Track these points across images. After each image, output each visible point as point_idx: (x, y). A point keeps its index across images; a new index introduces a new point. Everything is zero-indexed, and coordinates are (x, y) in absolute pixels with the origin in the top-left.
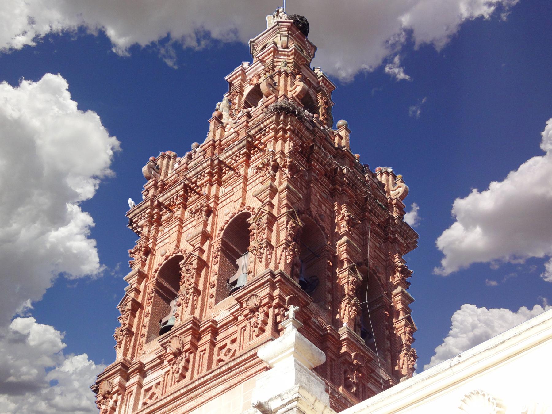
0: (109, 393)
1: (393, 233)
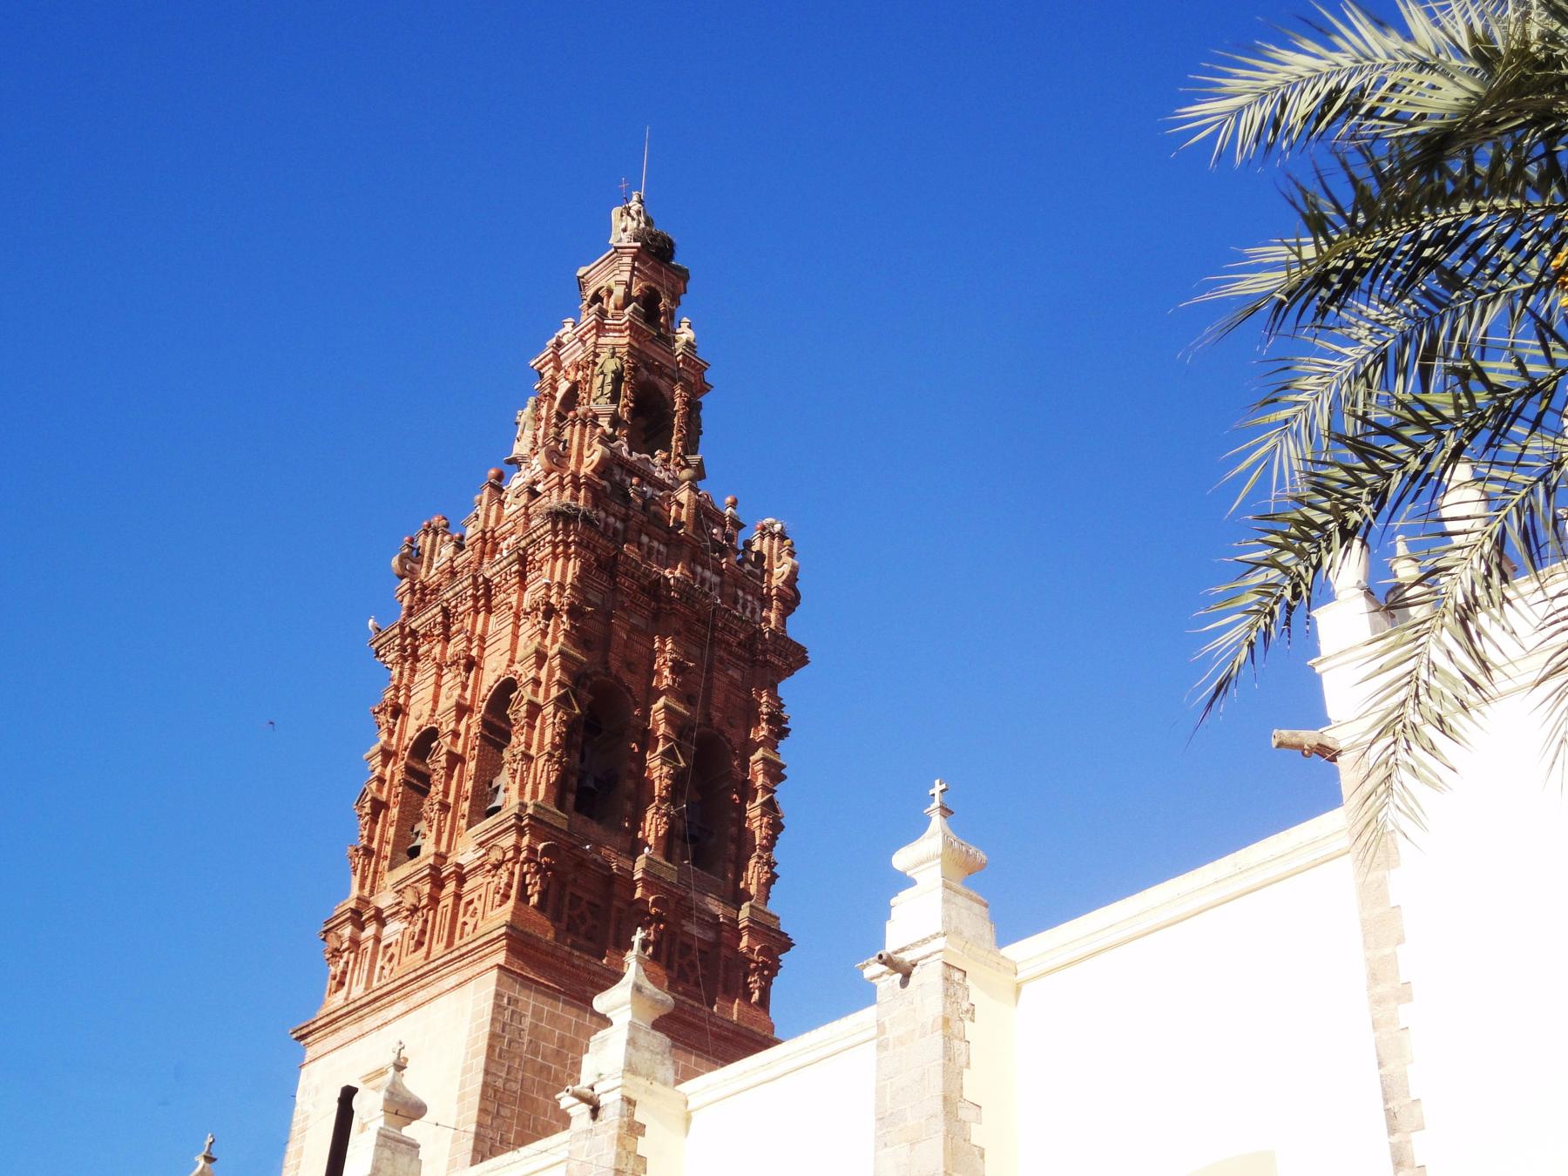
0: (337, 950)
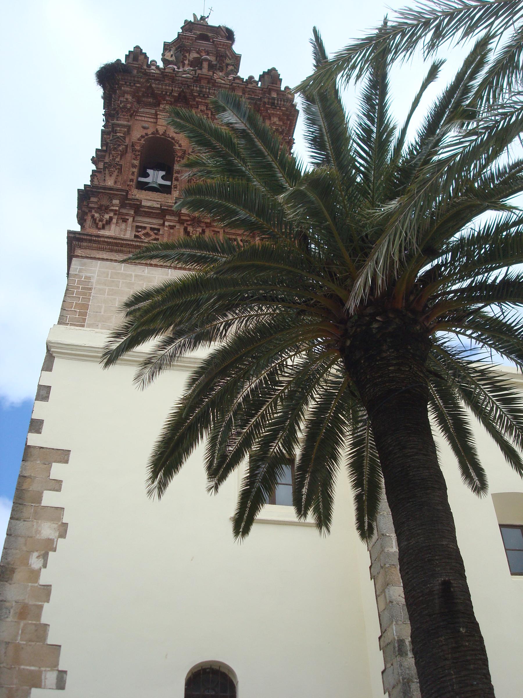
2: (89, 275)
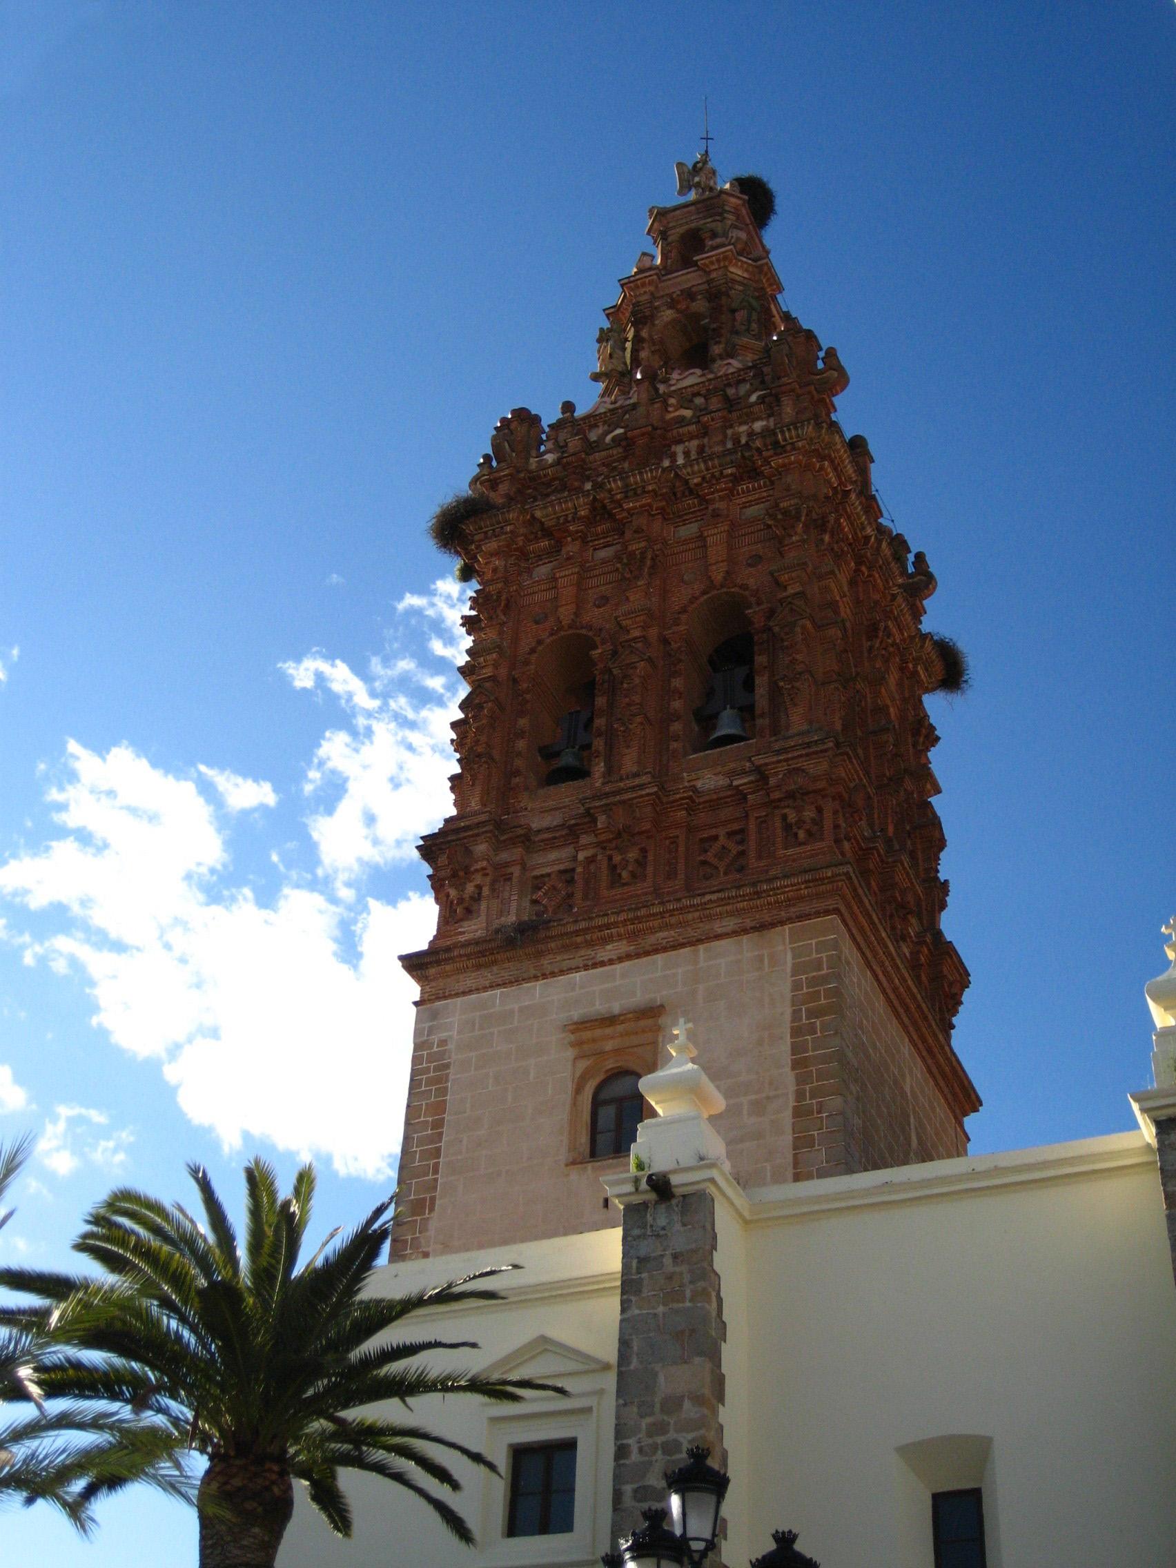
1: (917, 660)
2: (444, 1035)
